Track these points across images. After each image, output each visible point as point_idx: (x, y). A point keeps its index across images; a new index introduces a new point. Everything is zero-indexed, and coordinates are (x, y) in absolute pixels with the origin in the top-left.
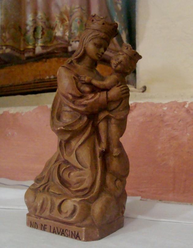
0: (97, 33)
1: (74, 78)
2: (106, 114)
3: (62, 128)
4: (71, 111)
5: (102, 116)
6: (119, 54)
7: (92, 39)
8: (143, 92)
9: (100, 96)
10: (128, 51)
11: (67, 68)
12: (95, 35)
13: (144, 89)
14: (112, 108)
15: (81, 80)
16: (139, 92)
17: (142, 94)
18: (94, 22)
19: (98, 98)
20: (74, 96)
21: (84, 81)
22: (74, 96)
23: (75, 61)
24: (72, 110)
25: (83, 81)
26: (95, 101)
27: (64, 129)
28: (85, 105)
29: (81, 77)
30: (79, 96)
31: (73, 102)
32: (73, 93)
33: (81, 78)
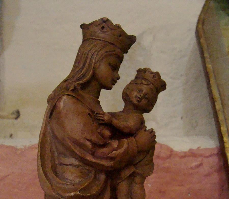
0: (111, 48)
1: (89, 115)
2: (133, 169)
3: (79, 193)
4: (79, 166)
5: (126, 173)
6: (142, 83)
7: (106, 56)
8: (17, 118)
9: (128, 144)
10: (155, 80)
11: (77, 98)
12: (109, 51)
13: (17, 114)
14: (137, 161)
15: (98, 118)
16: (12, 118)
17: (16, 121)
18: (105, 30)
19: (128, 147)
20: (95, 145)
21: (103, 120)
22: (95, 145)
23: (79, 87)
24: (81, 164)
25: (99, 120)
26: (125, 151)
27: (82, 194)
28: (111, 159)
29: (97, 114)
30: (102, 144)
31: (93, 154)
32: (94, 138)
33: (99, 115)
